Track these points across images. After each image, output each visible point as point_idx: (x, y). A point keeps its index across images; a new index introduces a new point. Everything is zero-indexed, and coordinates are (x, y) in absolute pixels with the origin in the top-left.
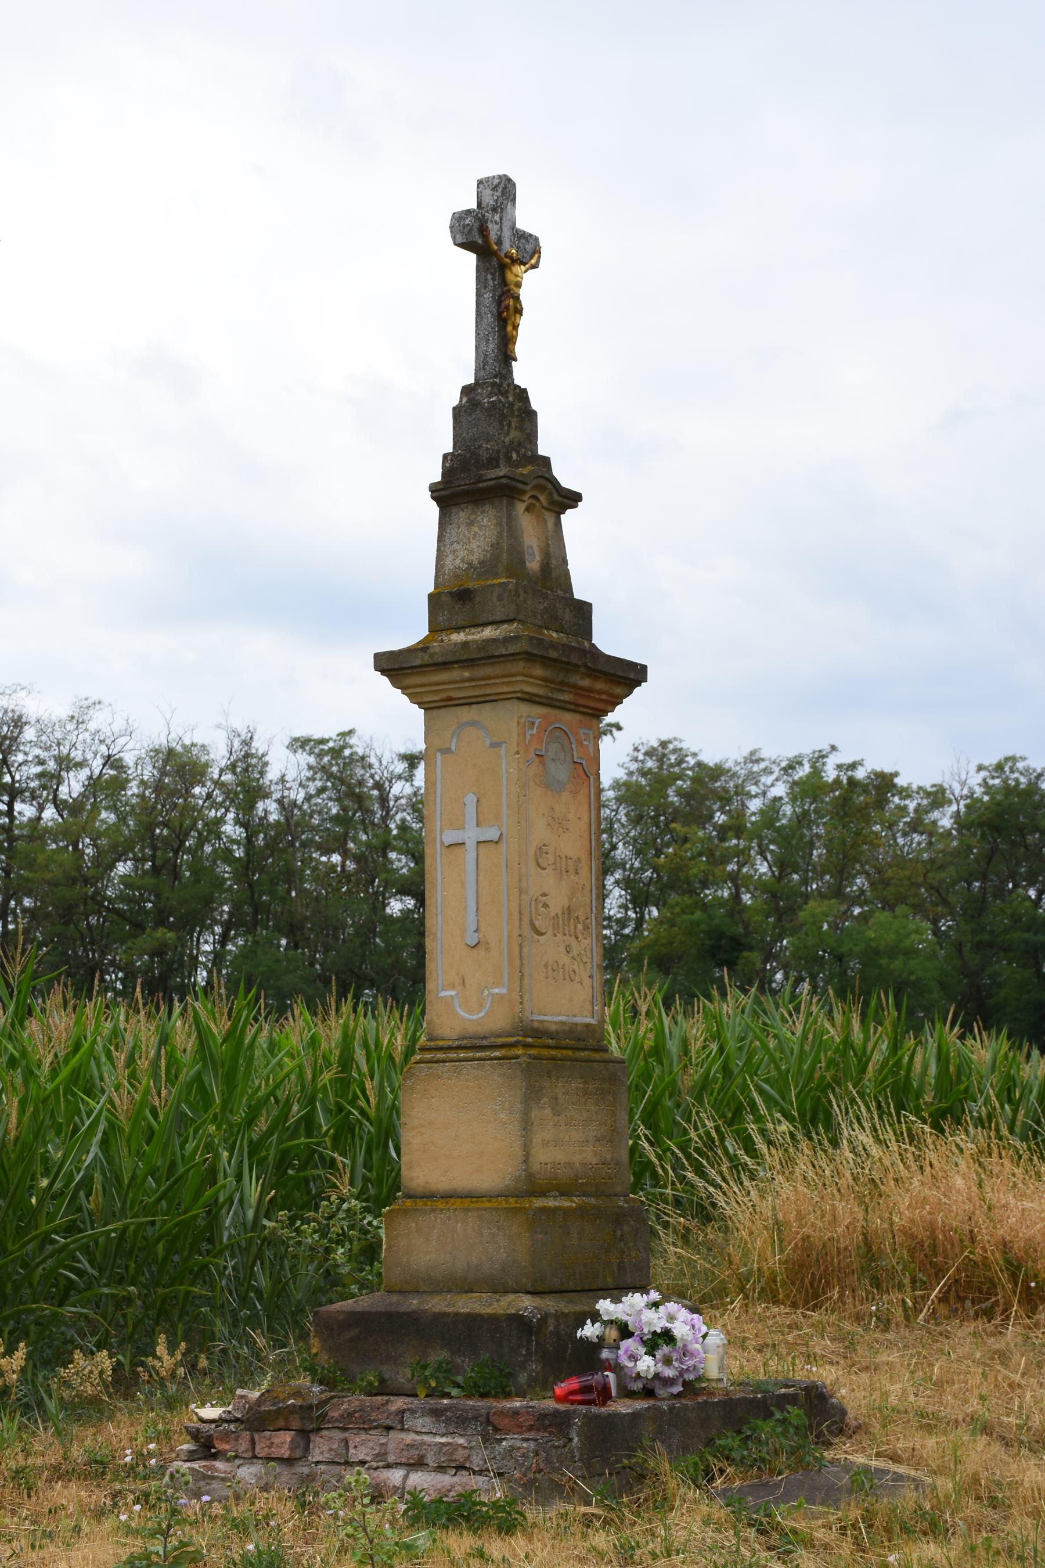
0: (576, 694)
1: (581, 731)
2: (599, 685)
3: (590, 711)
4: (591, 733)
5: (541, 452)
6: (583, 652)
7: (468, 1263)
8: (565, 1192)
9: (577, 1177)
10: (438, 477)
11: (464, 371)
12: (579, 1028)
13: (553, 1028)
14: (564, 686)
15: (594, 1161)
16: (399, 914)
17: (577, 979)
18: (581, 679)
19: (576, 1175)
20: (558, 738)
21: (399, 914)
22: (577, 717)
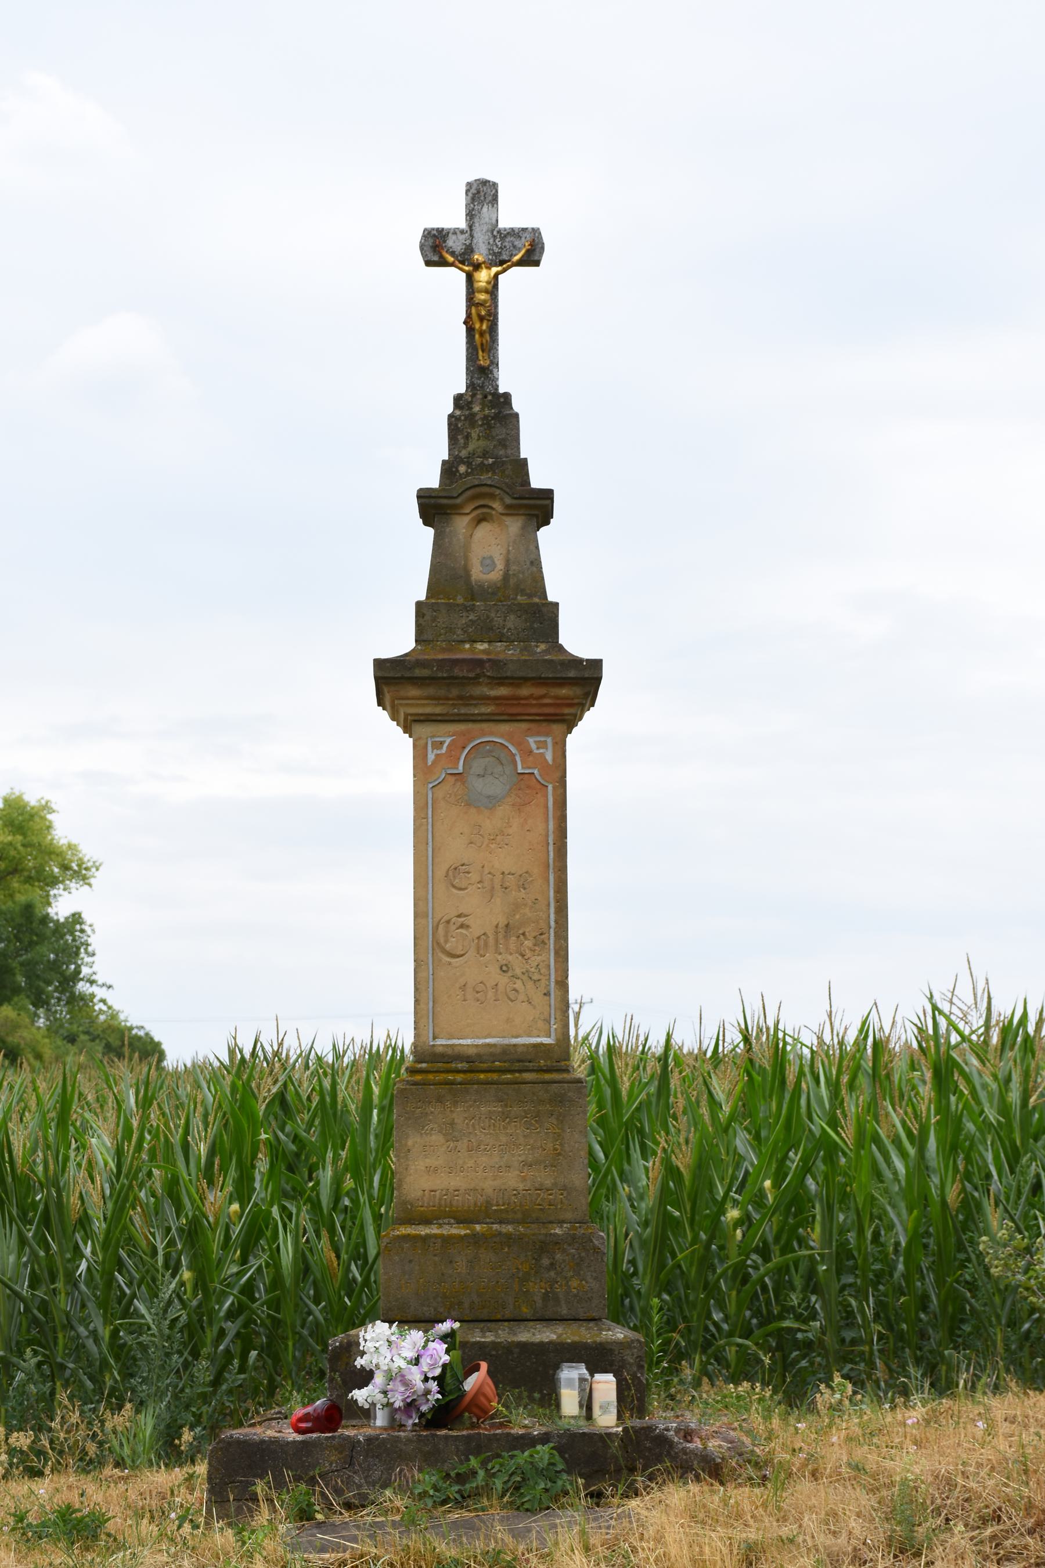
0: (497, 705)
1: (531, 740)
2: (525, 691)
3: (519, 718)
4: (549, 740)
5: (430, 532)
6: (562, 663)
7: (231, 1053)
8: (462, 1219)
9: (488, 1203)
10: (433, 481)
11: (457, 381)
12: (520, 1050)
13: (472, 1051)
14: (465, 700)
15: (521, 1186)
16: (359, 1367)
17: (522, 997)
18: (492, 689)
19: (488, 1202)
20: (490, 751)
21: (359, 1367)
22: (524, 726)
